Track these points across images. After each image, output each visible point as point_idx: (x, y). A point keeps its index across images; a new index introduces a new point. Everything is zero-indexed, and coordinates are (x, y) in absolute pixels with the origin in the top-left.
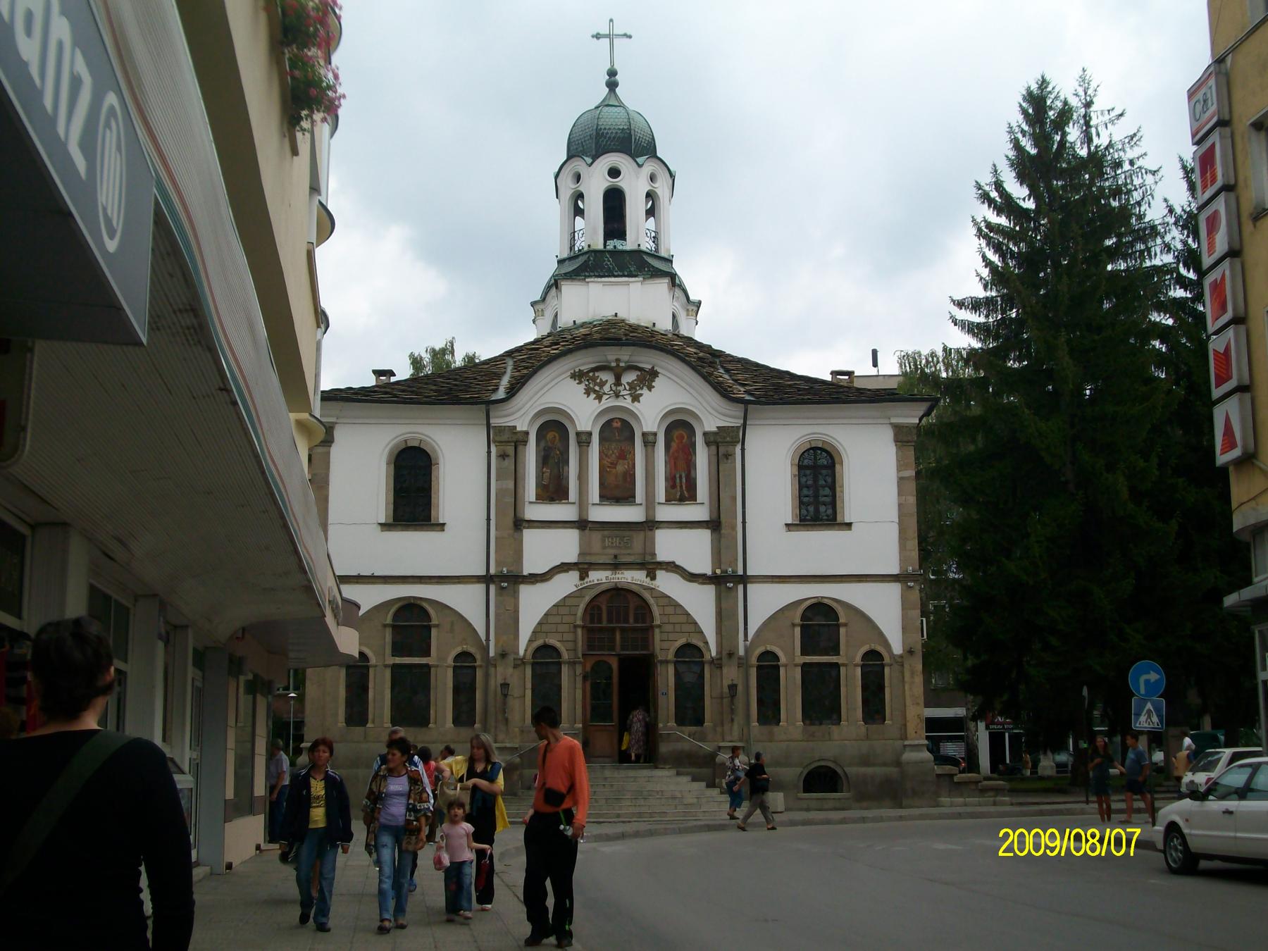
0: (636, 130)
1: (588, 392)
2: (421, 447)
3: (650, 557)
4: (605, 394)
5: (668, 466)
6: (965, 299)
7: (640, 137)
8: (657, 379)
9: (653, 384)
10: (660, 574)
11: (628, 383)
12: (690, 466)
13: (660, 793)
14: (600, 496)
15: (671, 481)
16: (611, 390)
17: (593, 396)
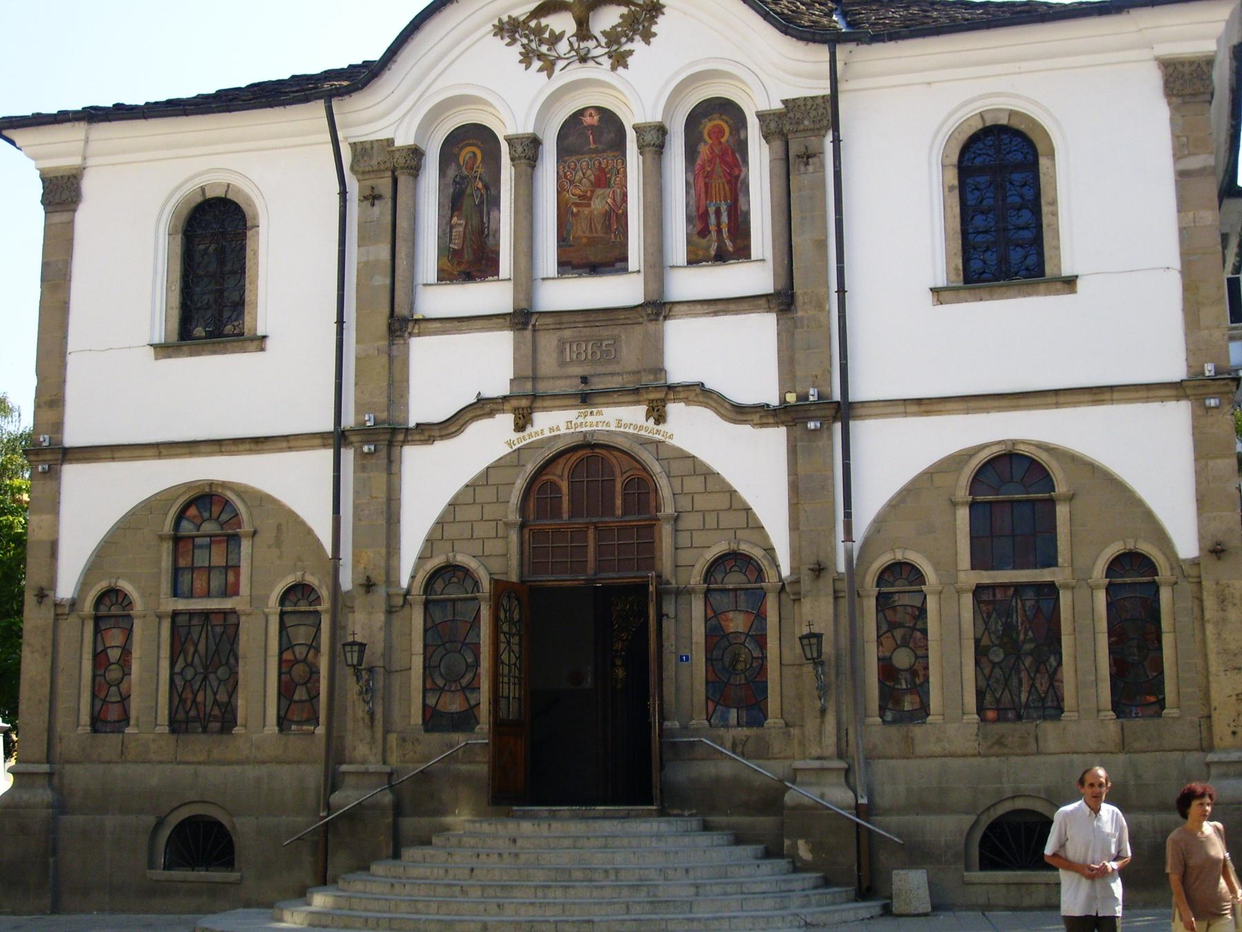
1: (527, 58)
2: (228, 197)
3: (652, 377)
5: (692, 192)
9: (654, 29)
10: (675, 410)
11: (604, 33)
12: (737, 186)
15: (699, 222)
16: (572, 48)
17: (537, 64)
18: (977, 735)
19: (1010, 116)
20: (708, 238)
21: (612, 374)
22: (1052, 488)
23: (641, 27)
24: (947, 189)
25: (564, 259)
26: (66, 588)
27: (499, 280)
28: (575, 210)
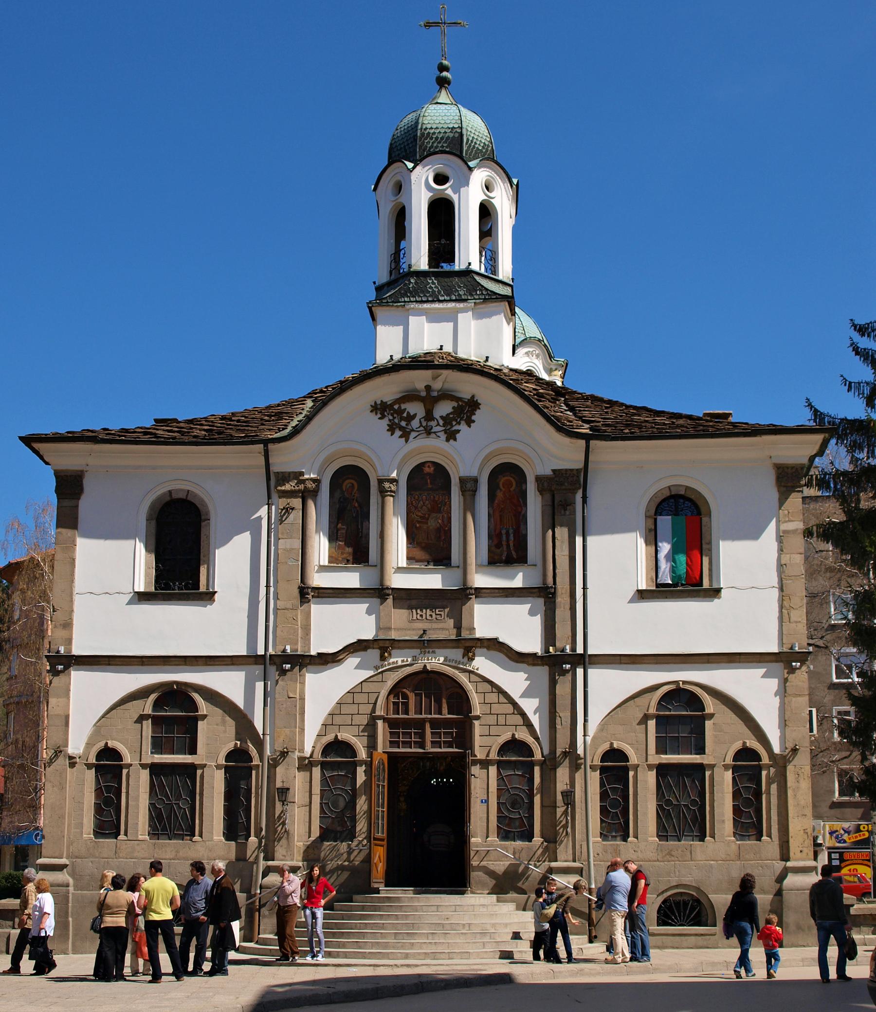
0: (469, 129)
1: (392, 429)
3: (468, 632)
5: (492, 520)
6: (868, 324)
8: (478, 412)
9: (473, 418)
11: (442, 417)
12: (521, 519)
14: (408, 558)
15: (495, 538)
16: (421, 425)
17: (398, 433)
19: (686, 489)
20: (501, 549)
21: (443, 629)
24: (647, 531)
25: (410, 556)
26: (76, 745)
28: (418, 525)
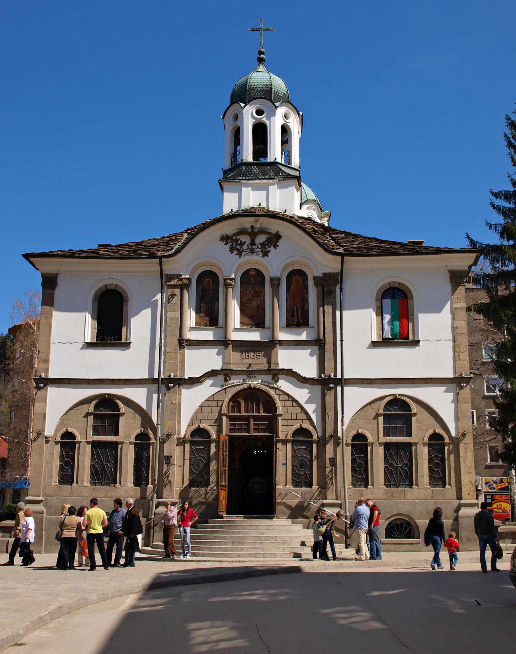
0: (276, 86)
1: (232, 250)
2: (116, 289)
3: (275, 366)
4: (244, 251)
5: (289, 301)
6: (500, 192)
7: (278, 90)
9: (278, 244)
11: (260, 244)
13: (274, 538)
14: (241, 323)
16: (248, 248)
17: (235, 252)
18: (385, 493)
21: (260, 364)
22: (410, 410)
23: (273, 243)
25: (242, 322)
27: (218, 327)
